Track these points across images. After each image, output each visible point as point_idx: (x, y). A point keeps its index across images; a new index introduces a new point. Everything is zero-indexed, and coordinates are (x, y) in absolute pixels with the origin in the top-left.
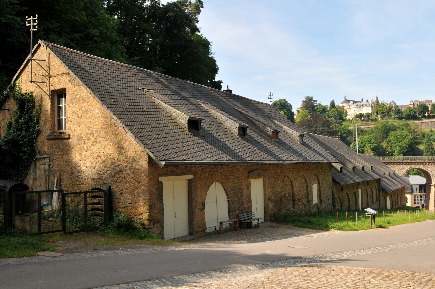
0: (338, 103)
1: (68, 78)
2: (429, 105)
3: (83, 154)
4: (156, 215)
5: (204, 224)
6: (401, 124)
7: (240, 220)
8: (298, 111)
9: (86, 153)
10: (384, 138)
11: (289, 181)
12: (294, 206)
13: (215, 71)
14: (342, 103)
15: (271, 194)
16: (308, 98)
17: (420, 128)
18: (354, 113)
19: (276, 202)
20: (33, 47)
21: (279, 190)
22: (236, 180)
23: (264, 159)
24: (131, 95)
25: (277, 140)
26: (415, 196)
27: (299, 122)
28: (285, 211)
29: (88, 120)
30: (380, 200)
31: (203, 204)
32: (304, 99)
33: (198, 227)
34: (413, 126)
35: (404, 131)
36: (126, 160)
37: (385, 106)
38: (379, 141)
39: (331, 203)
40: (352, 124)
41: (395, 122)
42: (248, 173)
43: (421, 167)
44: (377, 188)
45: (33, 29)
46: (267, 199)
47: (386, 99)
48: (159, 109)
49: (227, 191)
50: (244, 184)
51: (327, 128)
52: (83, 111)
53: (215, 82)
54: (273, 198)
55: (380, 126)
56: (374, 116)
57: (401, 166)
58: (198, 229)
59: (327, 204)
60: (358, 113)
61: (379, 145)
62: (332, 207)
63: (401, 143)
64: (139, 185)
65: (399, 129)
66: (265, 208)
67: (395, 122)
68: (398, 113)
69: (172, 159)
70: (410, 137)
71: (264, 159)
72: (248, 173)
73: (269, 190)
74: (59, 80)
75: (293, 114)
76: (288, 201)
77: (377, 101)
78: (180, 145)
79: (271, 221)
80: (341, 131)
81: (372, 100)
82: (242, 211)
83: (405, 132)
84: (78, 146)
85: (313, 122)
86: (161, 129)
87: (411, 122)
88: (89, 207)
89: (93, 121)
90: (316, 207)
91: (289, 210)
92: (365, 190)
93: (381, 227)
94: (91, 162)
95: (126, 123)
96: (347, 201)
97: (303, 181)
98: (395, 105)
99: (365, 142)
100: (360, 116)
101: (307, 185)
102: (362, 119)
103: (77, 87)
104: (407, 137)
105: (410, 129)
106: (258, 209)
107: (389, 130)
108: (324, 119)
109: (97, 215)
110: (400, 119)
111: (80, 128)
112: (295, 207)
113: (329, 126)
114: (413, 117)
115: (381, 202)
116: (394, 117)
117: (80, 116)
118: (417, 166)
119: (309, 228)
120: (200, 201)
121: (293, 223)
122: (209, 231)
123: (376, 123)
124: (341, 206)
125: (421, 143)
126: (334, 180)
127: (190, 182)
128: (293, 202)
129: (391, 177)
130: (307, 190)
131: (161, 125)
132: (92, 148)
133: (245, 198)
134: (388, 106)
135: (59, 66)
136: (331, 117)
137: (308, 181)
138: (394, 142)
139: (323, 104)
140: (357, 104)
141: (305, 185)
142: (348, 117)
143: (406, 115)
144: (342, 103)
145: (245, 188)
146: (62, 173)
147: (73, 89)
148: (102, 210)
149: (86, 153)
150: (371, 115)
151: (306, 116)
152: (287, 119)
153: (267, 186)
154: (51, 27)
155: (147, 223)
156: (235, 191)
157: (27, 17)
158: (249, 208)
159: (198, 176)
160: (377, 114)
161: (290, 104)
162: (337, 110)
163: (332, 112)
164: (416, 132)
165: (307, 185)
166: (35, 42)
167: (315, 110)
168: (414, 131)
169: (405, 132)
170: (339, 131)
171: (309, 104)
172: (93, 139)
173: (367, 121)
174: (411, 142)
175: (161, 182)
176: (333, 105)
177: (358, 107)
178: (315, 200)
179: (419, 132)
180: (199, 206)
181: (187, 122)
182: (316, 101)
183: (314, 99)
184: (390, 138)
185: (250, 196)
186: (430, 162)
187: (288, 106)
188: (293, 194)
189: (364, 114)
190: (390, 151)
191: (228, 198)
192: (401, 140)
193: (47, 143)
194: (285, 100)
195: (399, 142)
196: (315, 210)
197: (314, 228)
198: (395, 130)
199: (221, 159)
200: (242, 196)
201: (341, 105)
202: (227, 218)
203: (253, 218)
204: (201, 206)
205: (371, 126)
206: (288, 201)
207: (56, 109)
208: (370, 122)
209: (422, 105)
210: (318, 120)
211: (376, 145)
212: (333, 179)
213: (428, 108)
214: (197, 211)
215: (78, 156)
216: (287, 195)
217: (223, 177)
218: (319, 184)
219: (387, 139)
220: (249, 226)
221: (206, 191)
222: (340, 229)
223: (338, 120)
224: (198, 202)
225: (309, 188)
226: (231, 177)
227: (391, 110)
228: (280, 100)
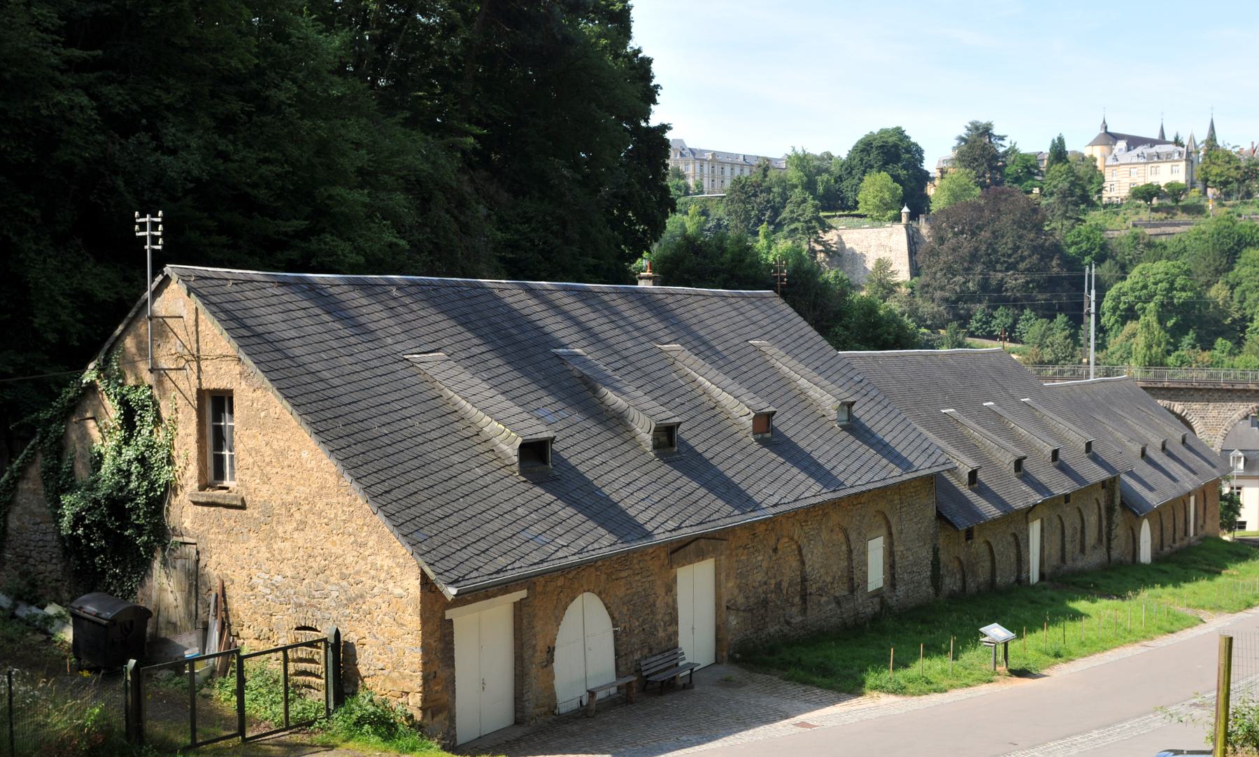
1: (238, 369)
3: (275, 547)
4: (438, 696)
5: (553, 696)
7: (645, 674)
8: (942, 171)
9: (282, 545)
10: (1218, 272)
11: (794, 547)
12: (804, 611)
13: (650, 95)
14: (1093, 144)
15: (736, 592)
16: (977, 128)
18: (1128, 180)
19: (751, 610)
20: (153, 281)
21: (759, 577)
22: (638, 578)
23: (715, 516)
24: (382, 389)
25: (769, 435)
27: (941, 211)
28: (777, 628)
29: (285, 471)
30: (1109, 540)
31: (551, 651)
33: (537, 706)
36: (373, 572)
38: (1203, 279)
39: (927, 581)
40: (1119, 219)
42: (672, 553)
44: (1103, 505)
45: (152, 230)
46: (723, 608)
48: (451, 415)
49: (613, 608)
50: (659, 582)
51: (1032, 236)
52: (274, 450)
53: (649, 129)
54: (741, 600)
55: (1211, 228)
58: (537, 711)
59: (912, 586)
60: (1141, 182)
61: (1200, 295)
62: (931, 590)
64: (400, 632)
66: (718, 629)
69: (475, 574)
71: (715, 516)
72: (672, 553)
73: (730, 585)
74: (218, 369)
75: (925, 178)
76: (787, 600)
77: (1212, 138)
78: (496, 525)
79: (732, 660)
81: (1192, 139)
82: (651, 650)
84: (264, 527)
85: (987, 213)
86: (453, 483)
88: (291, 669)
89: (298, 476)
90: (876, 600)
91: (788, 623)
92: (1057, 521)
93: (1022, 673)
94: (295, 567)
95: (373, 488)
96: (987, 564)
97: (841, 537)
99: (1156, 284)
100: (1147, 193)
101: (849, 546)
102: (1155, 201)
103: (259, 393)
106: (696, 637)
107: (1239, 243)
108: (1022, 203)
109: (309, 686)
111: (267, 487)
112: (809, 612)
113: (1038, 228)
115: (1114, 543)
117: (267, 460)
119: (819, 687)
120: (541, 645)
121: (785, 670)
122: (563, 709)
123: (1201, 219)
124: (964, 582)
126: (940, 516)
127: (518, 607)
128: (804, 598)
129: (1171, 455)
130: (850, 559)
131: (453, 471)
132: (296, 535)
133: (659, 617)
134: (1243, 164)
135: (215, 335)
136: (1052, 194)
137: (853, 536)
139: (1025, 148)
140: (1140, 149)
141: (844, 548)
144: (1093, 144)
145: (661, 591)
146: (226, 584)
147: (251, 395)
148: (319, 677)
149: (282, 545)
151: (965, 189)
152: (756, 446)
153: (723, 576)
154: (167, 99)
155: (418, 716)
156: (634, 605)
157: (137, 214)
158: (670, 640)
159: (539, 589)
162: (1071, 171)
165: (849, 546)
166: (157, 269)
171: (980, 149)
172: (297, 516)
175: (451, 621)
176: (1059, 153)
178: (876, 577)
180: (540, 656)
181: (516, 452)
182: (1002, 138)
183: (996, 131)
184: (1241, 271)
185: (675, 609)
187: (908, 150)
188: (804, 580)
189: (1159, 187)
190: (1237, 316)
191: (614, 626)
193: (191, 510)
194: (899, 132)
196: (871, 608)
197: (830, 688)
199: (596, 546)
200: (653, 613)
201: (1087, 152)
202: (611, 677)
203: (681, 664)
204: (545, 655)
205: (1183, 229)
206: (787, 600)
207: (209, 432)
208: (1181, 217)
210: (1003, 207)
211: (1189, 294)
212: (938, 512)
214: (534, 670)
215: (264, 549)
216: (785, 585)
217: (603, 577)
218: (890, 534)
219: (1231, 275)
220: (669, 687)
221: (558, 620)
222: (900, 690)
223: (1070, 207)
224: (538, 648)
225: (855, 553)
226: (624, 574)
228: (884, 132)
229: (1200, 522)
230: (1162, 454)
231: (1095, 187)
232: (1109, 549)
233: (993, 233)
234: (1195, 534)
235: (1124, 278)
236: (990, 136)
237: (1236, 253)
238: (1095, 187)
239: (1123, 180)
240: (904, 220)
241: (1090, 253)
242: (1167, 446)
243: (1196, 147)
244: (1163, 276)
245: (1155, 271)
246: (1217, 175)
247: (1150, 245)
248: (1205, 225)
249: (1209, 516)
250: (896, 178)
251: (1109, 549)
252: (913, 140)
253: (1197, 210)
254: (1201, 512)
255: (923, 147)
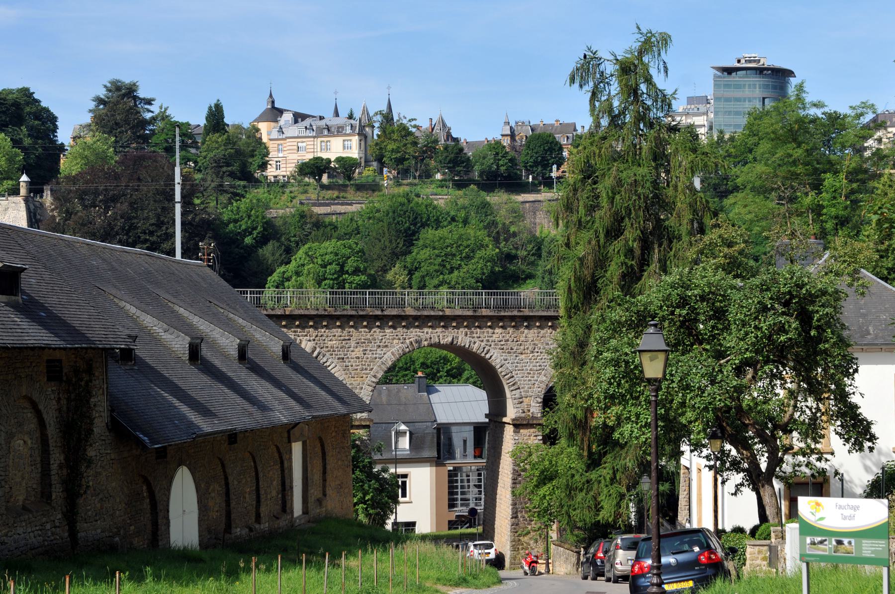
0: (236, 117)
2: (564, 142)
6: (461, 202)
10: (396, 256)
16: (118, 89)
17: (527, 222)
26: (452, 475)
32: (102, 93)
34: (503, 212)
35: (470, 231)
37: (410, 134)
38: (378, 264)
40: (285, 197)
41: (439, 195)
43: (462, 337)
44: (50, 417)
47: (418, 112)
56: (367, 173)
57: (377, 333)
60: (308, 157)
63: (456, 273)
65: (453, 219)
67: (439, 195)
68: (456, 160)
70: (491, 251)
77: (388, 117)
80: (236, 221)
81: (365, 111)
83: (474, 232)
87: (497, 199)
98: (449, 135)
100: (315, 168)
102: (325, 179)
104: (479, 254)
105: (494, 223)
110: (460, 185)
114: (512, 183)
116: (438, 176)
118: (445, 336)
123: (376, 197)
125: (530, 276)
134: (421, 142)
138: (432, 268)
139: (178, 115)
140: (307, 122)
142: (271, 172)
143: (482, 173)
150: (359, 165)
151: (102, 157)
160: (382, 164)
161: (47, 110)
163: (209, 150)
164: (514, 235)
167: (145, 139)
168: (506, 229)
169: (474, 232)
170: (229, 222)
171: (121, 109)
173: (343, 188)
174: (492, 272)
176: (216, 116)
177: (308, 133)
179: (525, 236)
182: (149, 102)
183: (142, 93)
184: (420, 254)
186: (501, 318)
192: (456, 262)
195: (451, 271)
198: (438, 224)
205: (354, 207)
208: (351, 194)
209: (539, 136)
210: (143, 174)
213: (561, 149)
219: (409, 259)
227: (430, 148)
229: (315, 493)
230: (236, 364)
231: (257, 161)
232: (71, 516)
233: (131, 204)
234: (305, 511)
235: (288, 262)
236: (135, 98)
237: (414, 233)
238: (257, 161)
239: (291, 156)
240: (23, 191)
241: (251, 233)
242: (250, 354)
243: (370, 119)
244: (332, 256)
245: (322, 251)
246: (393, 151)
247: (318, 224)
248: (377, 202)
249: (332, 483)
250: (16, 143)
251: (71, 516)
252: (43, 104)
253: (373, 187)
254: (316, 477)
255: (56, 114)
